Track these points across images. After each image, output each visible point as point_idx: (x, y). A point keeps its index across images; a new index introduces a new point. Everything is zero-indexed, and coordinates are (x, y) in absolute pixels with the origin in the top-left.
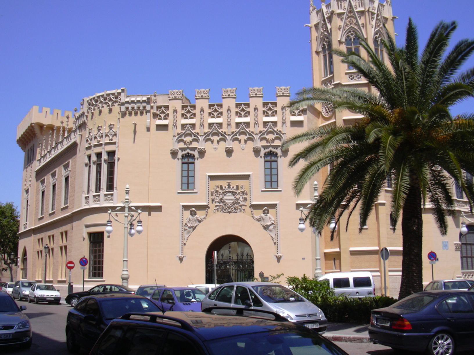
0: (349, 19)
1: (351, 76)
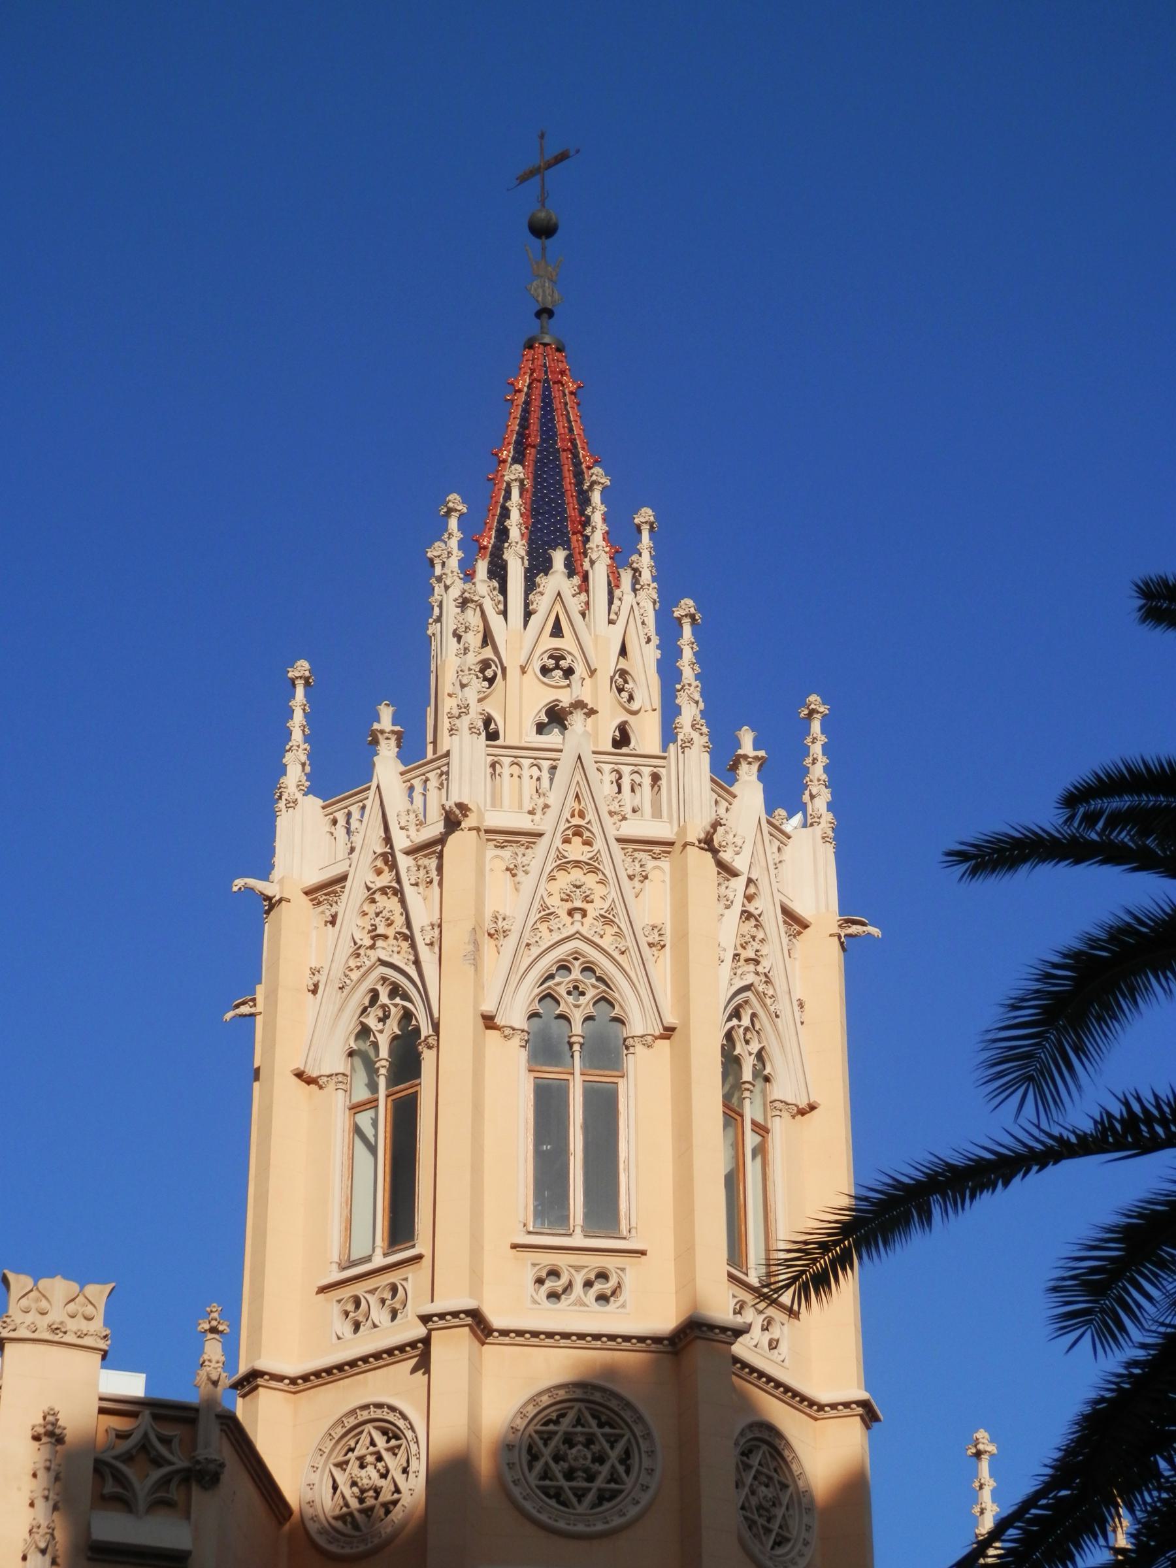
0: (564, 880)
1: (554, 1273)
